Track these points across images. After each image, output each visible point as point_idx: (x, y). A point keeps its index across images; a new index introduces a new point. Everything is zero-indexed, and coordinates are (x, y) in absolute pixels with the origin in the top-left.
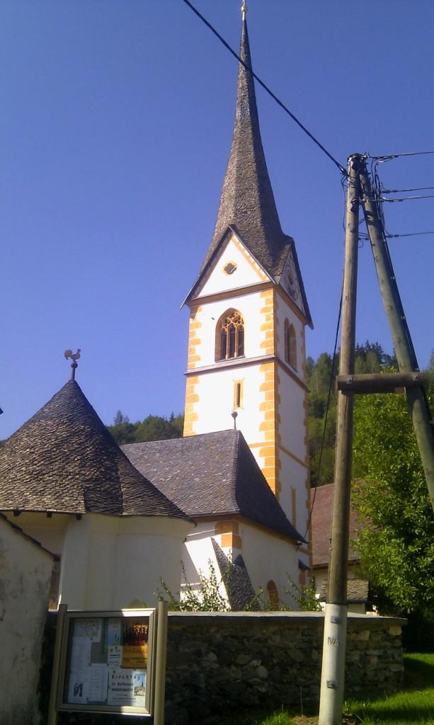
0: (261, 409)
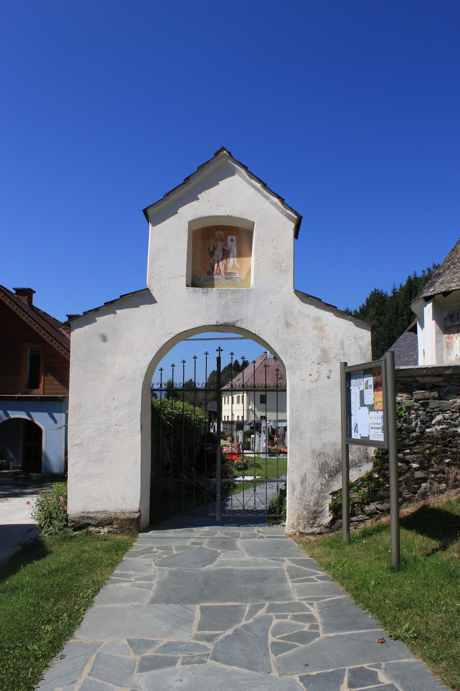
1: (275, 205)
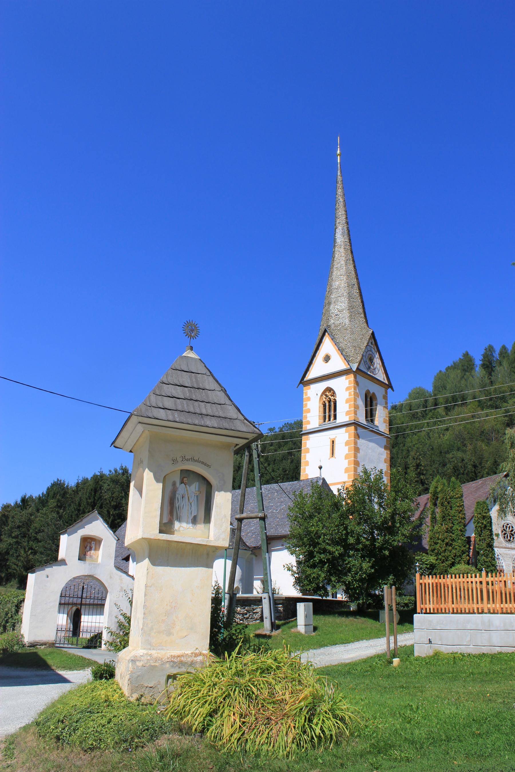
0: (346, 459)
1: (111, 533)
